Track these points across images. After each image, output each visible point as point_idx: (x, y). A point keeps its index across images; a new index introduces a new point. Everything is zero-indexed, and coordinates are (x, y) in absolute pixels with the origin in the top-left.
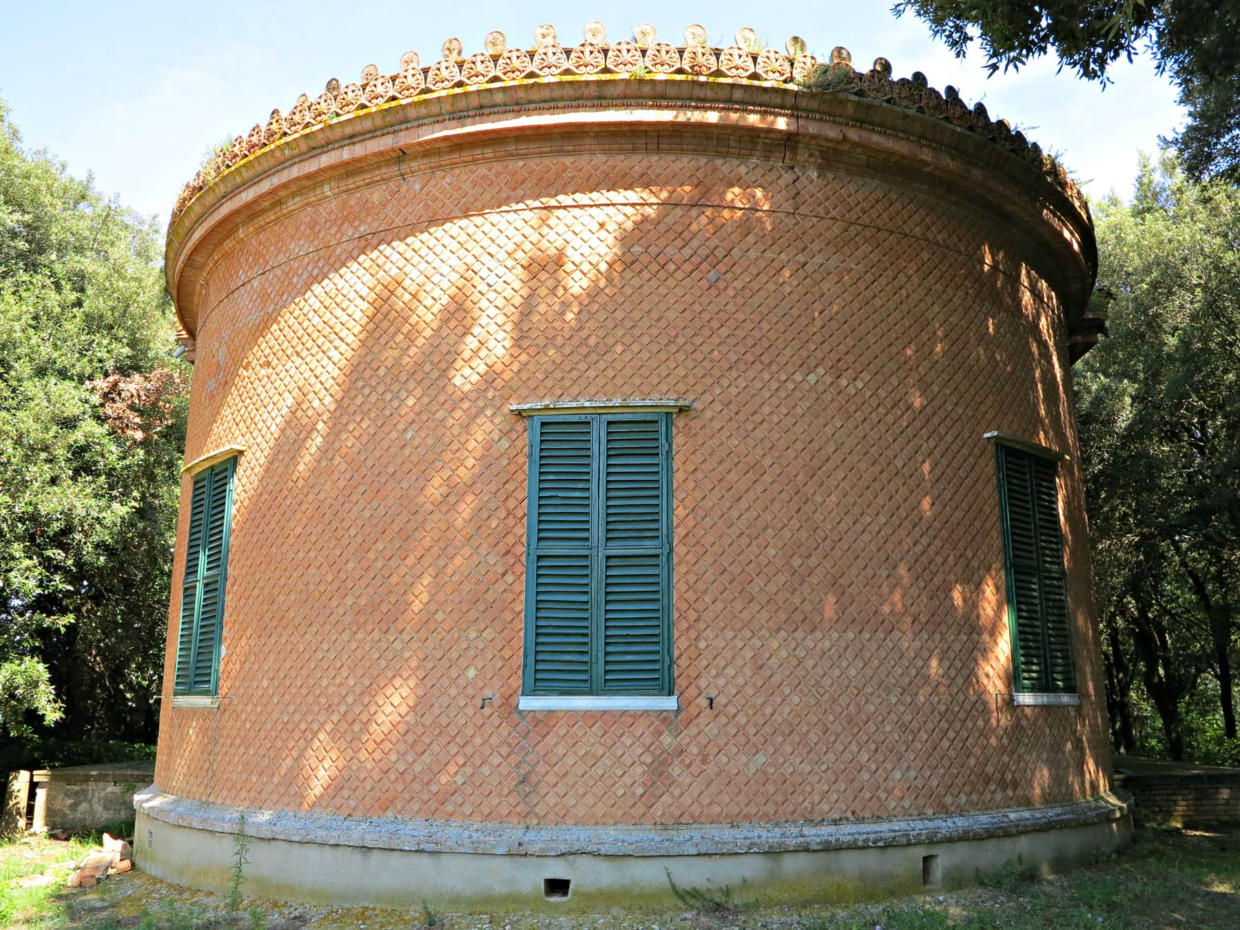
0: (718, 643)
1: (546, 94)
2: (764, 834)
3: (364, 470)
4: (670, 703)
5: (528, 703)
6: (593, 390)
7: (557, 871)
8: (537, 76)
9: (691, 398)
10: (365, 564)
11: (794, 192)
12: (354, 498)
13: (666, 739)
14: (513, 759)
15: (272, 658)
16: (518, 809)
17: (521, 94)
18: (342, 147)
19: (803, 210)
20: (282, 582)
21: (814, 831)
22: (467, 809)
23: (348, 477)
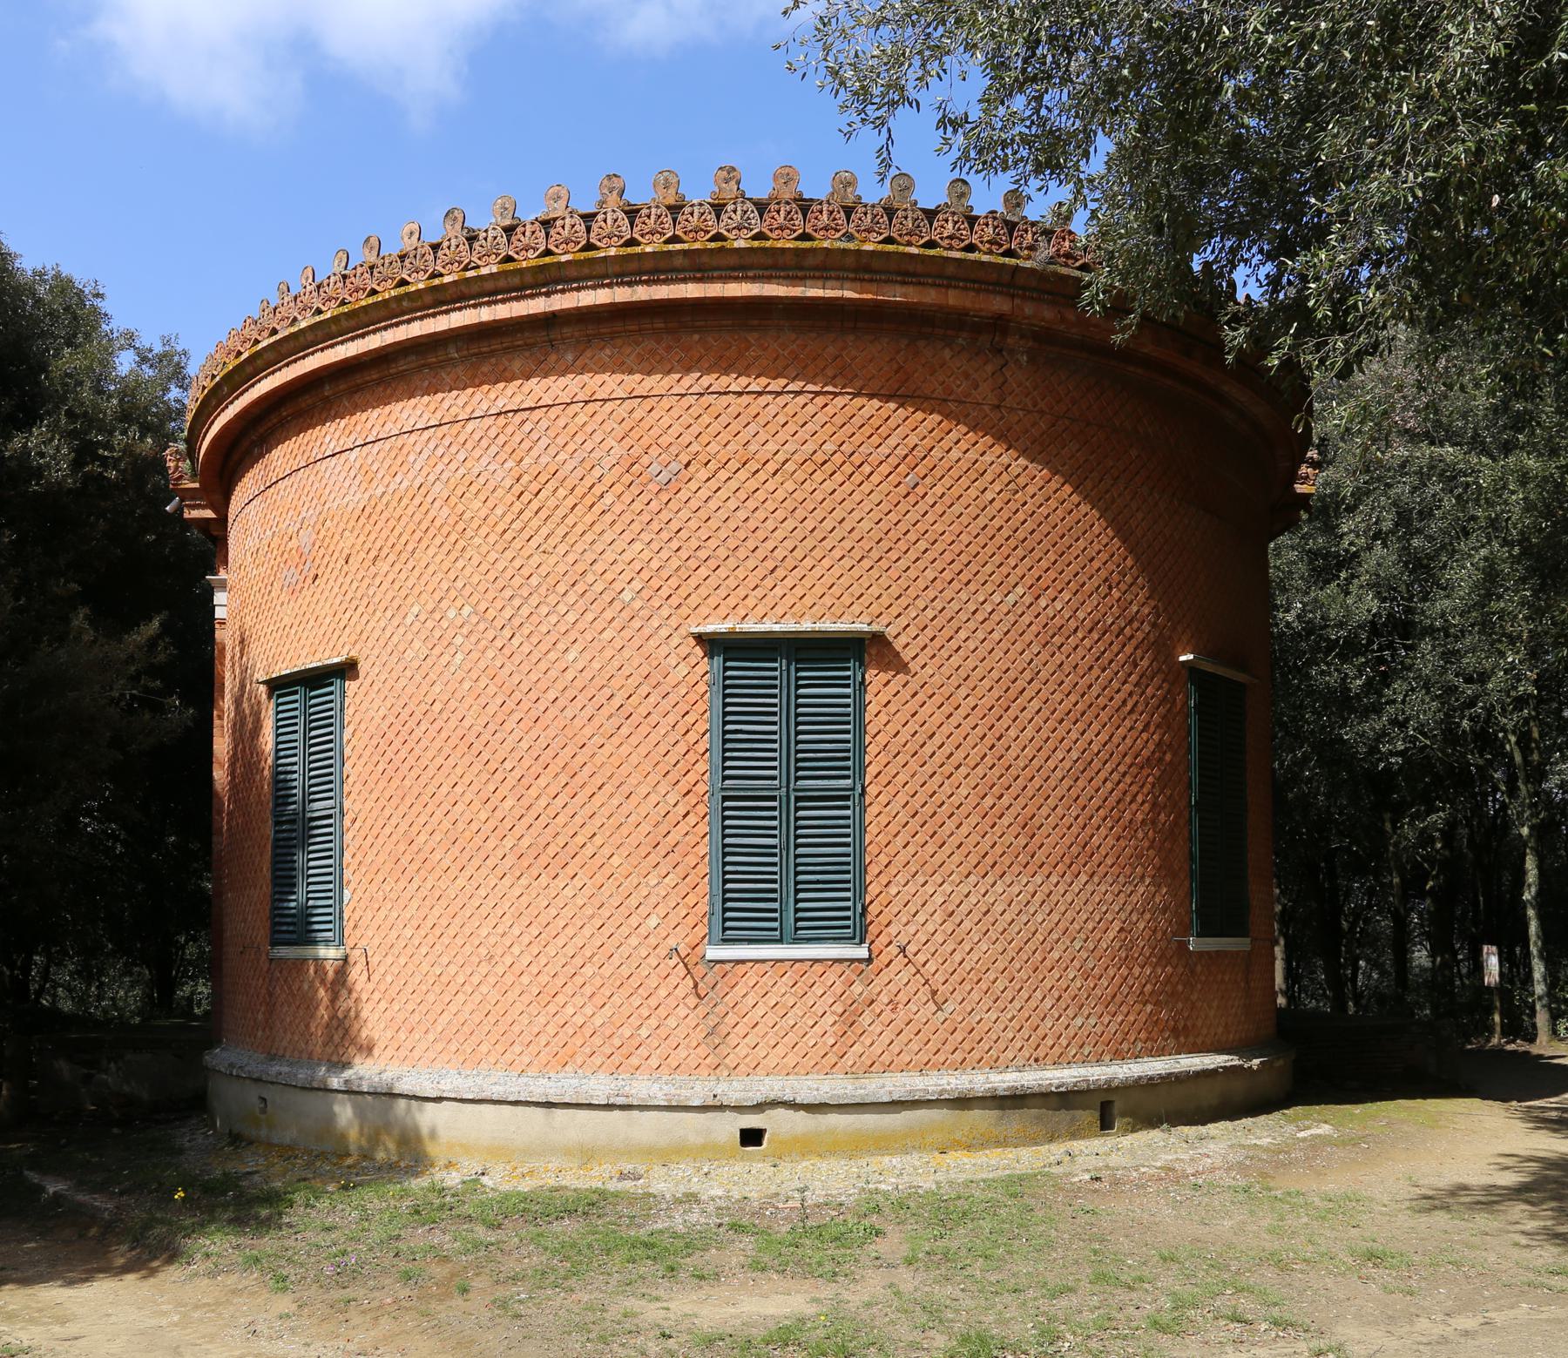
0: (912, 890)
1: (733, 260)
2: (953, 1081)
3: (517, 695)
4: (862, 952)
5: (714, 953)
6: (779, 610)
7: (752, 1121)
8: (724, 239)
9: (885, 622)
10: (525, 802)
11: (1001, 380)
12: (508, 726)
13: (857, 988)
14: (701, 1010)
15: (415, 903)
16: (708, 1061)
17: (705, 259)
18: (481, 305)
19: (1009, 402)
20: (422, 819)
21: (1000, 1077)
22: (654, 1062)
23: (499, 702)
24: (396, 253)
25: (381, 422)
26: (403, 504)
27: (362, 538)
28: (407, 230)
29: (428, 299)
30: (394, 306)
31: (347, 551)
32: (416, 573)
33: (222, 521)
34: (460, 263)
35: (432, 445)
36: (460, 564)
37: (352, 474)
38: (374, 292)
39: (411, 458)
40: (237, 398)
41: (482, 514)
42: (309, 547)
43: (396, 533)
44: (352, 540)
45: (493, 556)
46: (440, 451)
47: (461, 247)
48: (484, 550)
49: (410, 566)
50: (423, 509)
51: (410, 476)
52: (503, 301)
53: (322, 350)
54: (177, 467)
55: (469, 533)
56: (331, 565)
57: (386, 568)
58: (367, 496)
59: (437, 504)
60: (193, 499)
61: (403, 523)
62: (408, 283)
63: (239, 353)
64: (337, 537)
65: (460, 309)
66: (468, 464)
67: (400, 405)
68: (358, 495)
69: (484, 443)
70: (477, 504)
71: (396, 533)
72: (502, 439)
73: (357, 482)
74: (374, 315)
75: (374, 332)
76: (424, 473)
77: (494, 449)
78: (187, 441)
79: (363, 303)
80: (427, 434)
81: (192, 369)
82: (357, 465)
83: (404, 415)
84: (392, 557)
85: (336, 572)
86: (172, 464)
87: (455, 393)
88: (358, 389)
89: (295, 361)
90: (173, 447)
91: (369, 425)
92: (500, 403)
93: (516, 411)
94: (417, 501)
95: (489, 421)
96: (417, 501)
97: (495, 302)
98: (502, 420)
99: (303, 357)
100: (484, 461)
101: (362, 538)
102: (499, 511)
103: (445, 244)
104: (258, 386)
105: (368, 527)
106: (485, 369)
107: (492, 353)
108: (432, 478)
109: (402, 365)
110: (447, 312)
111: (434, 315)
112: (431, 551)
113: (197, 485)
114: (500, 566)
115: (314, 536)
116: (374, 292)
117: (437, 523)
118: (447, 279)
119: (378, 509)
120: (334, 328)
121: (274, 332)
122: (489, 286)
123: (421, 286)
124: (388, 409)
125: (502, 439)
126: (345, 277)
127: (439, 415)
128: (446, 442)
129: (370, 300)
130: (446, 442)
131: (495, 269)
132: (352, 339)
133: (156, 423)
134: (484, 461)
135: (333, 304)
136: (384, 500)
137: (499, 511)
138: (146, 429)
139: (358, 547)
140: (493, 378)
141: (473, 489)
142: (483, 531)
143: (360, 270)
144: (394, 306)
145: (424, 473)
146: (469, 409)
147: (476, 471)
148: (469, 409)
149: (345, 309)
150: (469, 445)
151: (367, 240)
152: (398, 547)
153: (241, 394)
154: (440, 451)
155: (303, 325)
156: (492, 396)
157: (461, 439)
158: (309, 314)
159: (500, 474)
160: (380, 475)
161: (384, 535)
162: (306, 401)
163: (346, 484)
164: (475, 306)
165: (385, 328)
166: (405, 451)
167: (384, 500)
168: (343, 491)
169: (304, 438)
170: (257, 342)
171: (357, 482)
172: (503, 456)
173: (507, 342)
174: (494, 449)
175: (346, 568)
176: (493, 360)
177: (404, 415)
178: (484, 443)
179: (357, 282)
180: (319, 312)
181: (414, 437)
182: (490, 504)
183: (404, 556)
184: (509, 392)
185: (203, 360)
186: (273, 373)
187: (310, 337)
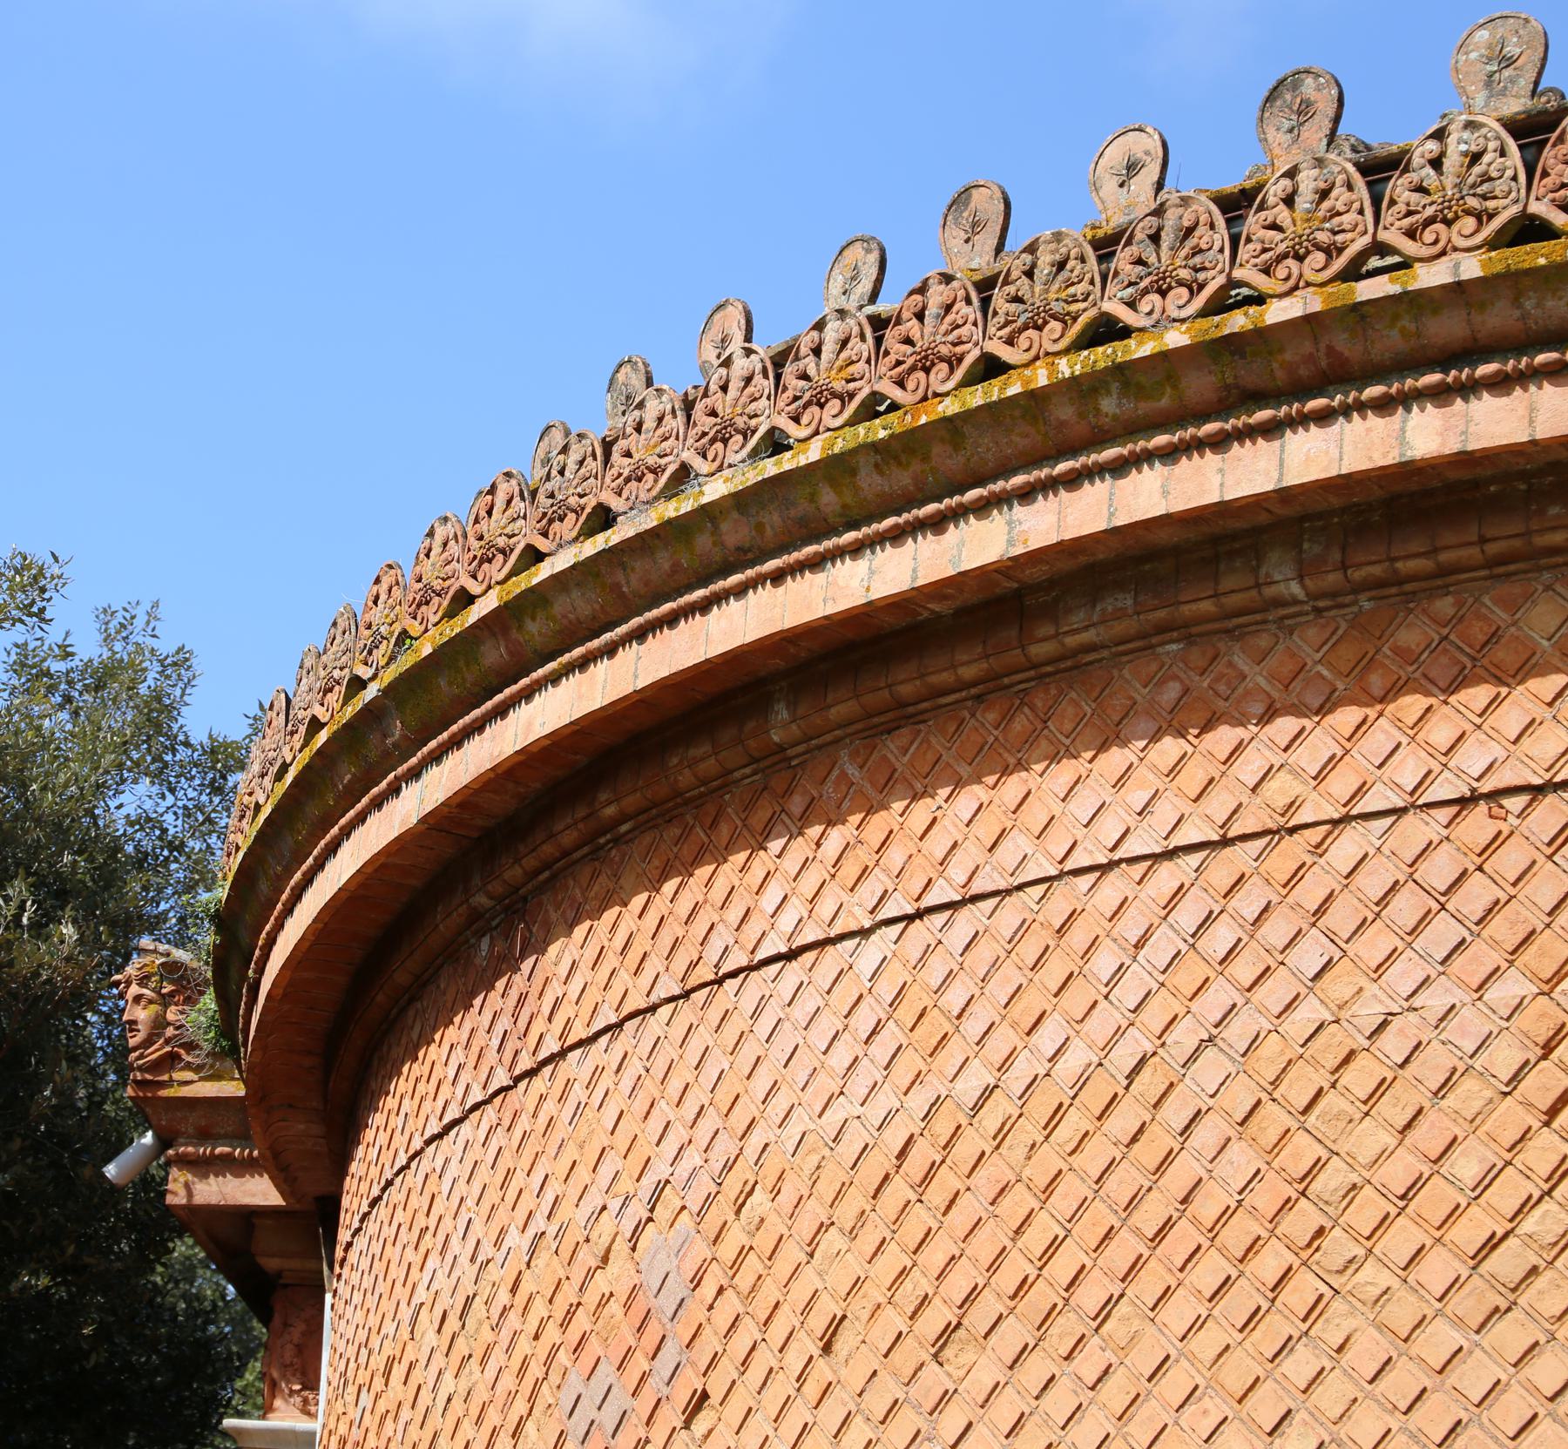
18: (1405, 400)
24: (1077, 235)
25: (986, 829)
26: (1067, 1132)
27: (894, 1259)
28: (1115, 155)
29: (1199, 385)
30: (1064, 412)
31: (827, 1308)
32: (1116, 1393)
33: (315, 1219)
34: (1331, 251)
35: (1188, 915)
36: (1300, 1365)
37: (864, 1020)
38: (991, 368)
39: (1104, 963)
40: (436, 757)
41: (1397, 1173)
42: (677, 1288)
43: (1035, 1239)
44: (854, 1265)
45: (1440, 1339)
46: (1221, 938)
47: (1339, 197)
48: (1402, 1313)
49: (1088, 1364)
50: (1148, 1152)
51: (1101, 1024)
52: (1501, 384)
53: (777, 578)
54: (159, 1024)
55: (1338, 1247)
56: (764, 1359)
57: (987, 1373)
58: (919, 1101)
59: (1206, 1136)
60: (205, 1136)
61: (1063, 1202)
62: (1125, 332)
63: (464, 599)
64: (793, 1253)
65: (1324, 418)
66: (1338, 986)
67: (1065, 772)
68: (885, 1100)
69: (1406, 908)
70: (1372, 1137)
71: (1035, 1239)
72: (1477, 895)
73: (881, 1049)
74: (986, 448)
75: (982, 508)
76: (1154, 1017)
77: (1443, 933)
78: (223, 919)
79: (950, 407)
80: (1167, 877)
81: (205, 717)
82: (886, 989)
83: (1082, 807)
84: (1014, 1334)
85: (782, 1386)
86: (142, 1015)
87: (1285, 726)
88: (902, 716)
89: (671, 620)
90: (151, 951)
91: (937, 844)
92: (1473, 759)
93: (1537, 791)
94: (1123, 1122)
95: (1417, 830)
96: (1123, 1122)
97: (1468, 390)
98: (1478, 826)
99: (704, 607)
100: (1404, 976)
101: (894, 1259)
102: (1466, 1166)
103: (1276, 190)
104: (523, 713)
105: (920, 1219)
106: (1411, 635)
107: (1443, 578)
108: (1185, 1037)
109: (1081, 628)
110: (1270, 430)
111: (1219, 443)
112: (1179, 1312)
113: (233, 1088)
114: (1474, 1377)
115: (701, 1250)
116: (991, 368)
117: (1207, 1208)
118: (1278, 312)
119: (965, 1150)
120: (828, 499)
121: (603, 518)
122: (1448, 328)
123: (1176, 338)
124: (1014, 786)
125: (1477, 895)
126: (879, 324)
127: (1219, 805)
128: (1248, 903)
129: (976, 397)
130: (1248, 903)
131: (1471, 268)
132: (896, 536)
133: (101, 889)
134: (1404, 976)
135: (831, 414)
136: (991, 1118)
137: (1466, 1166)
138: (56, 895)
139: (875, 1293)
140: (1442, 670)
141: (1360, 1078)
142: (1401, 1240)
143: (937, 296)
144: (1064, 412)
145: (1154, 1017)
146: (1341, 784)
147: (1368, 1012)
148: (1341, 784)
149: (878, 430)
150: (1341, 918)
151: (961, 199)
152: (1041, 1296)
153: (456, 742)
154: (1221, 938)
155: (715, 490)
156: (1440, 732)
157: (1310, 893)
158: (736, 452)
159: (1470, 1025)
160: (973, 1027)
161: (984, 1247)
162: (691, 766)
163: (841, 1057)
164: (1383, 406)
165: (1026, 495)
166: (1078, 937)
167: (991, 1118)
168: (826, 1084)
169: (676, 898)
170: (534, 556)
171: (881, 1049)
172: (1479, 958)
173: (1504, 535)
174: (1443, 933)
175: (822, 1371)
176: (1445, 606)
177: (1082, 807)
178: (1406, 908)
179: (927, 334)
180: (775, 444)
181: (1113, 888)
182: (1429, 1136)
183: (1066, 1328)
184: (1510, 718)
185: (253, 667)
186: (583, 664)
187: (735, 533)
